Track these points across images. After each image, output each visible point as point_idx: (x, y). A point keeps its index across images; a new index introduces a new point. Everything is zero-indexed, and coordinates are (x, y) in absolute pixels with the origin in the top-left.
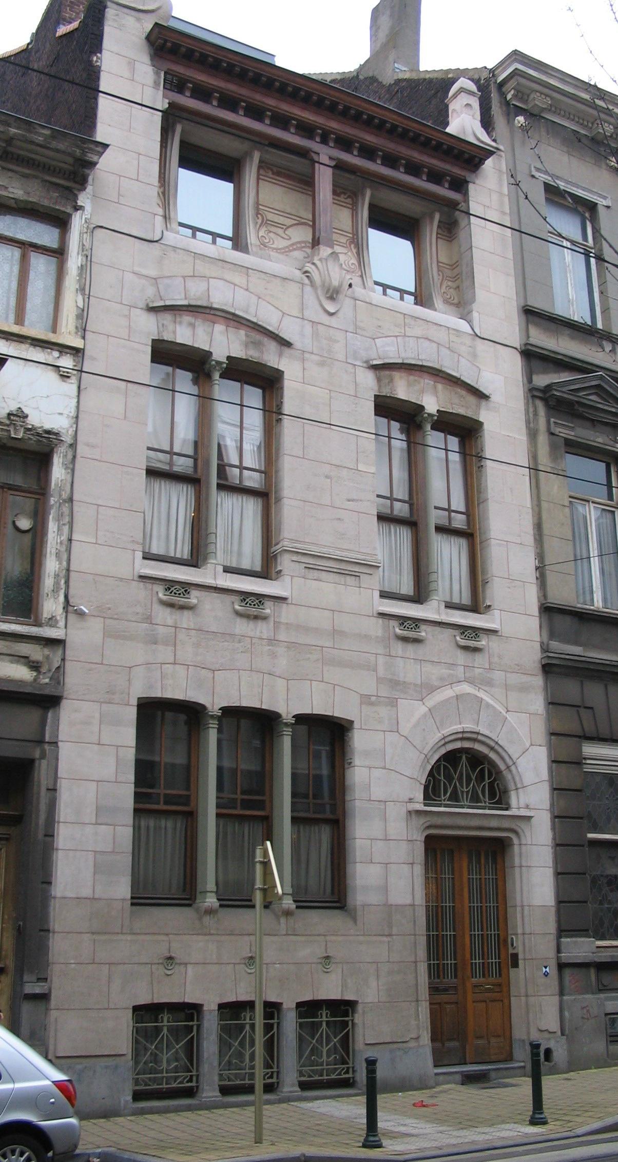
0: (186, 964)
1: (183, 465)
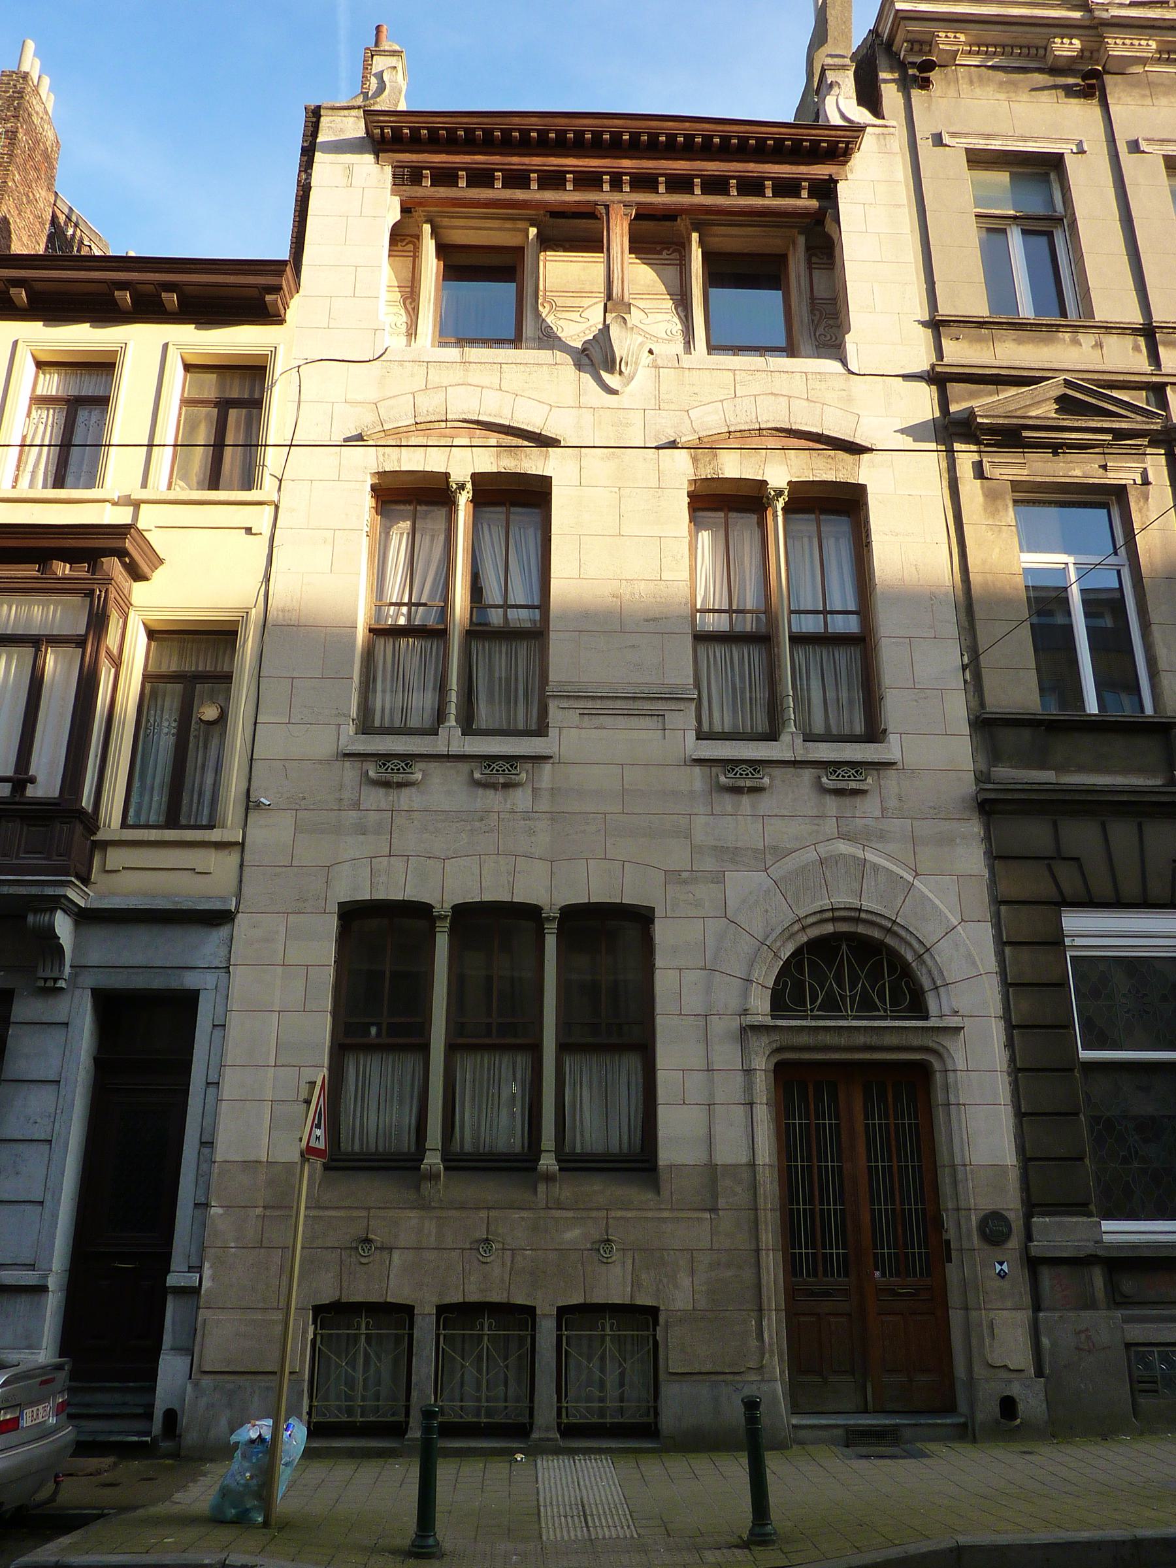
1: (748, 624)
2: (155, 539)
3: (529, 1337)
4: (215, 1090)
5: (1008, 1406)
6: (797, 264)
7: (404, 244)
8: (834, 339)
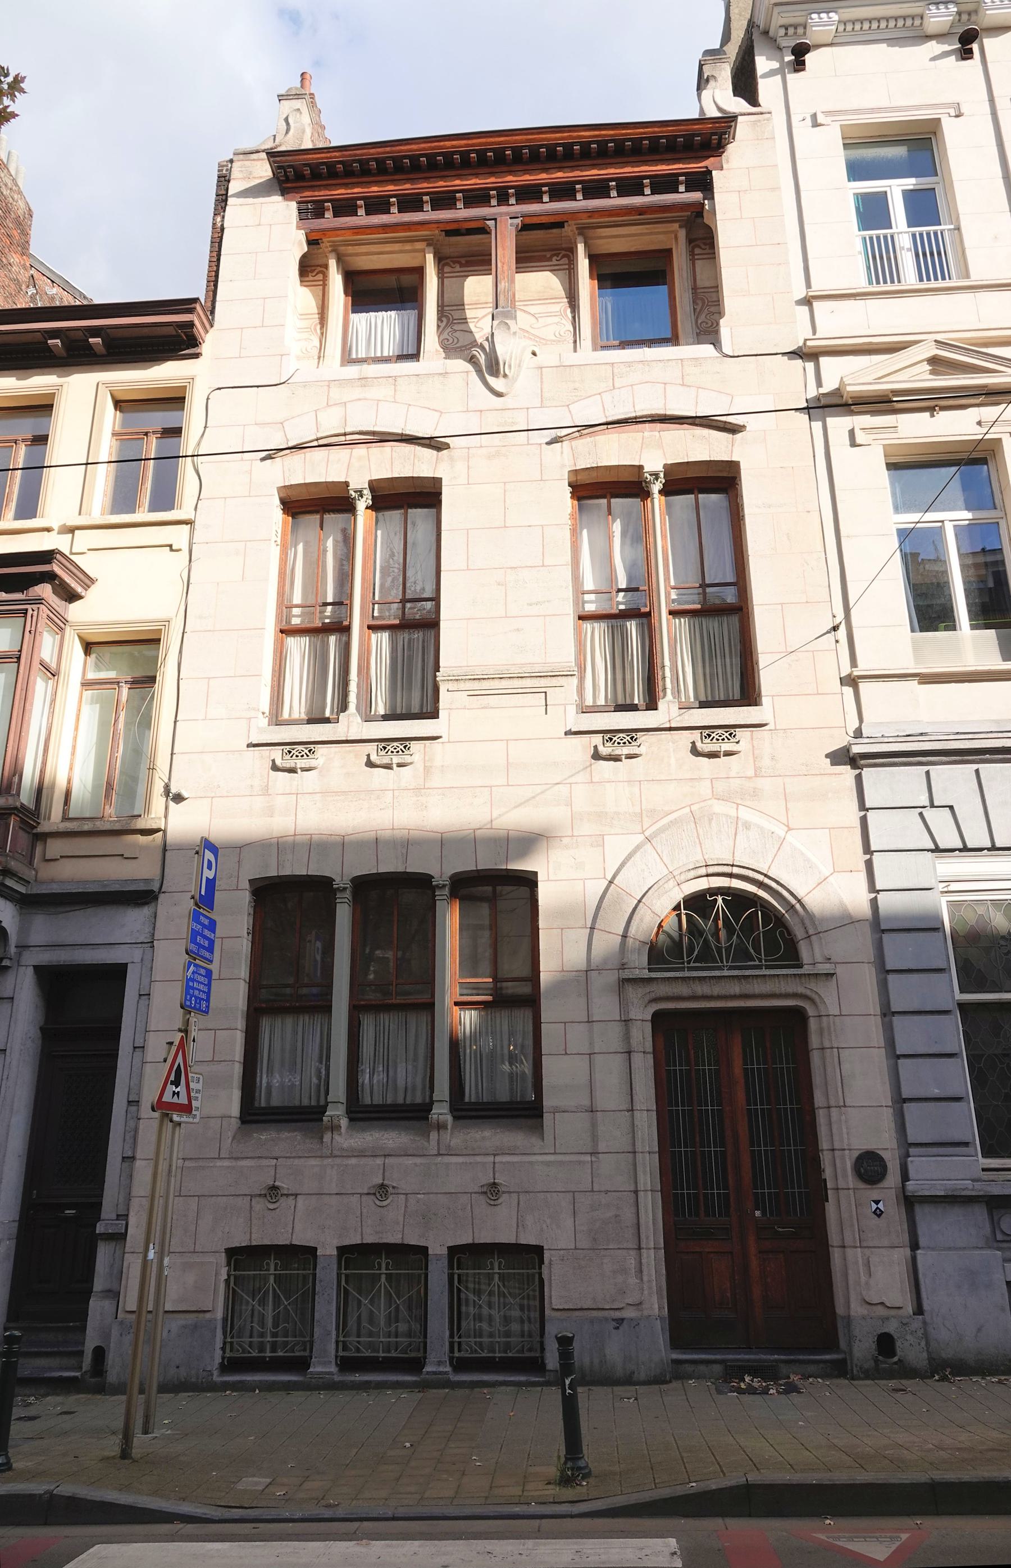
2: (85, 563)
4: (141, 1054)
5: (886, 1343)
7: (314, 274)
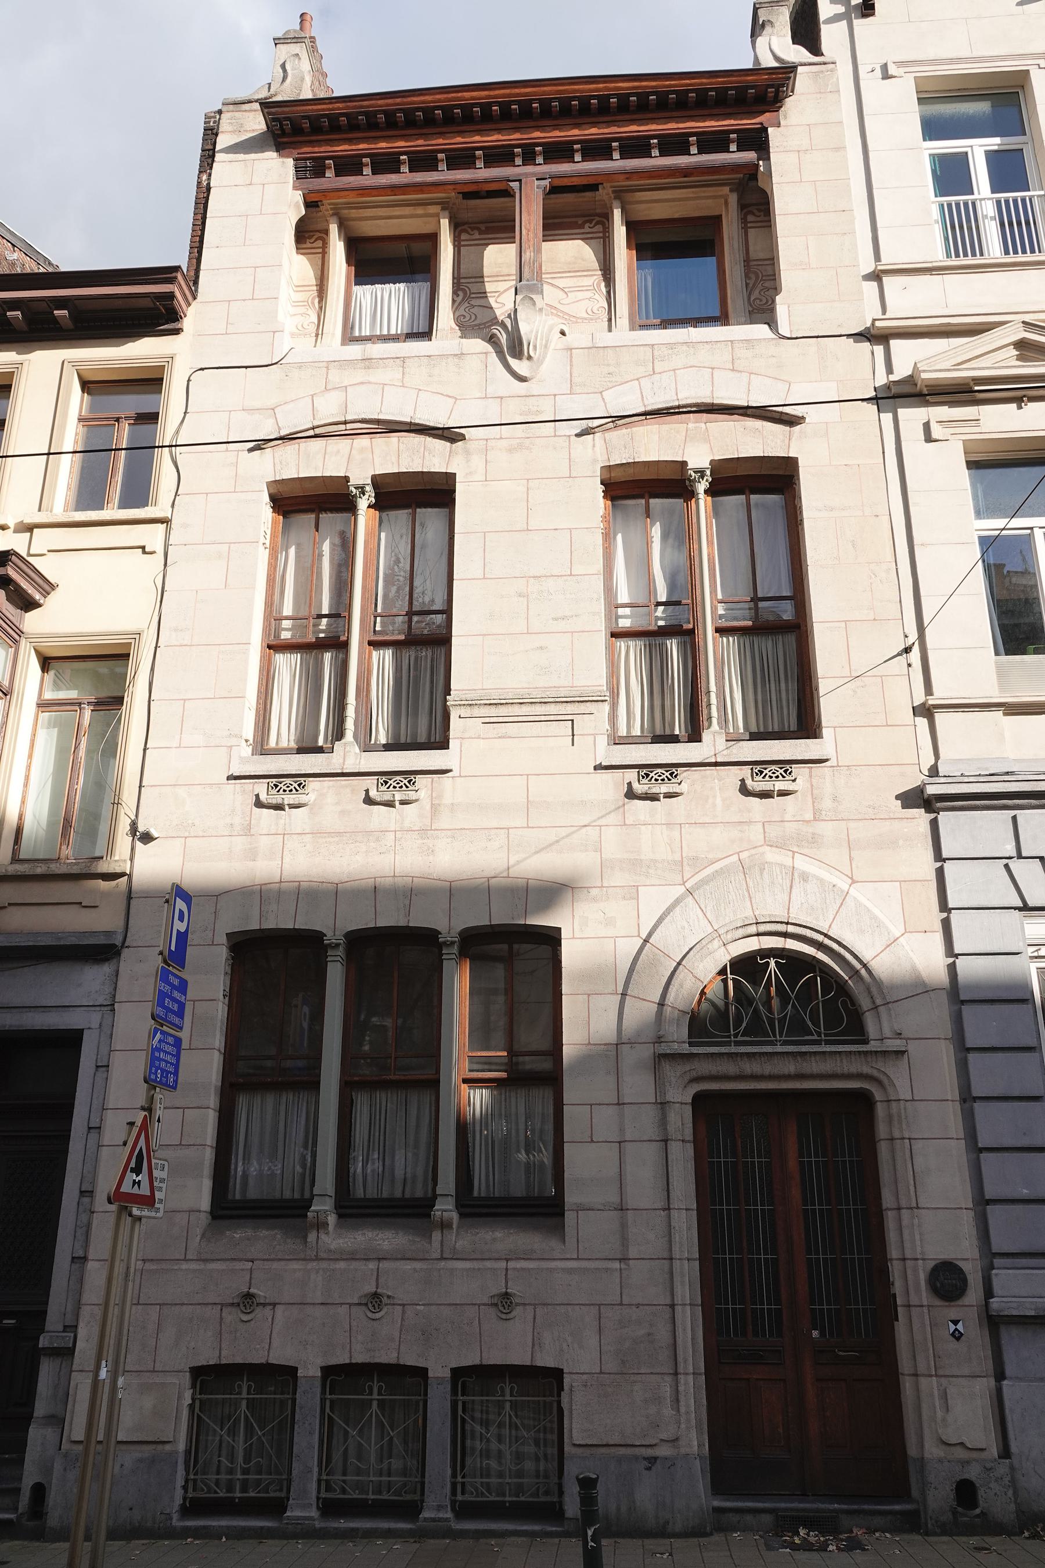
0: (274, 1305)
3: (290, 1402)
6: (730, 229)
7: (312, 241)
8: (770, 303)
